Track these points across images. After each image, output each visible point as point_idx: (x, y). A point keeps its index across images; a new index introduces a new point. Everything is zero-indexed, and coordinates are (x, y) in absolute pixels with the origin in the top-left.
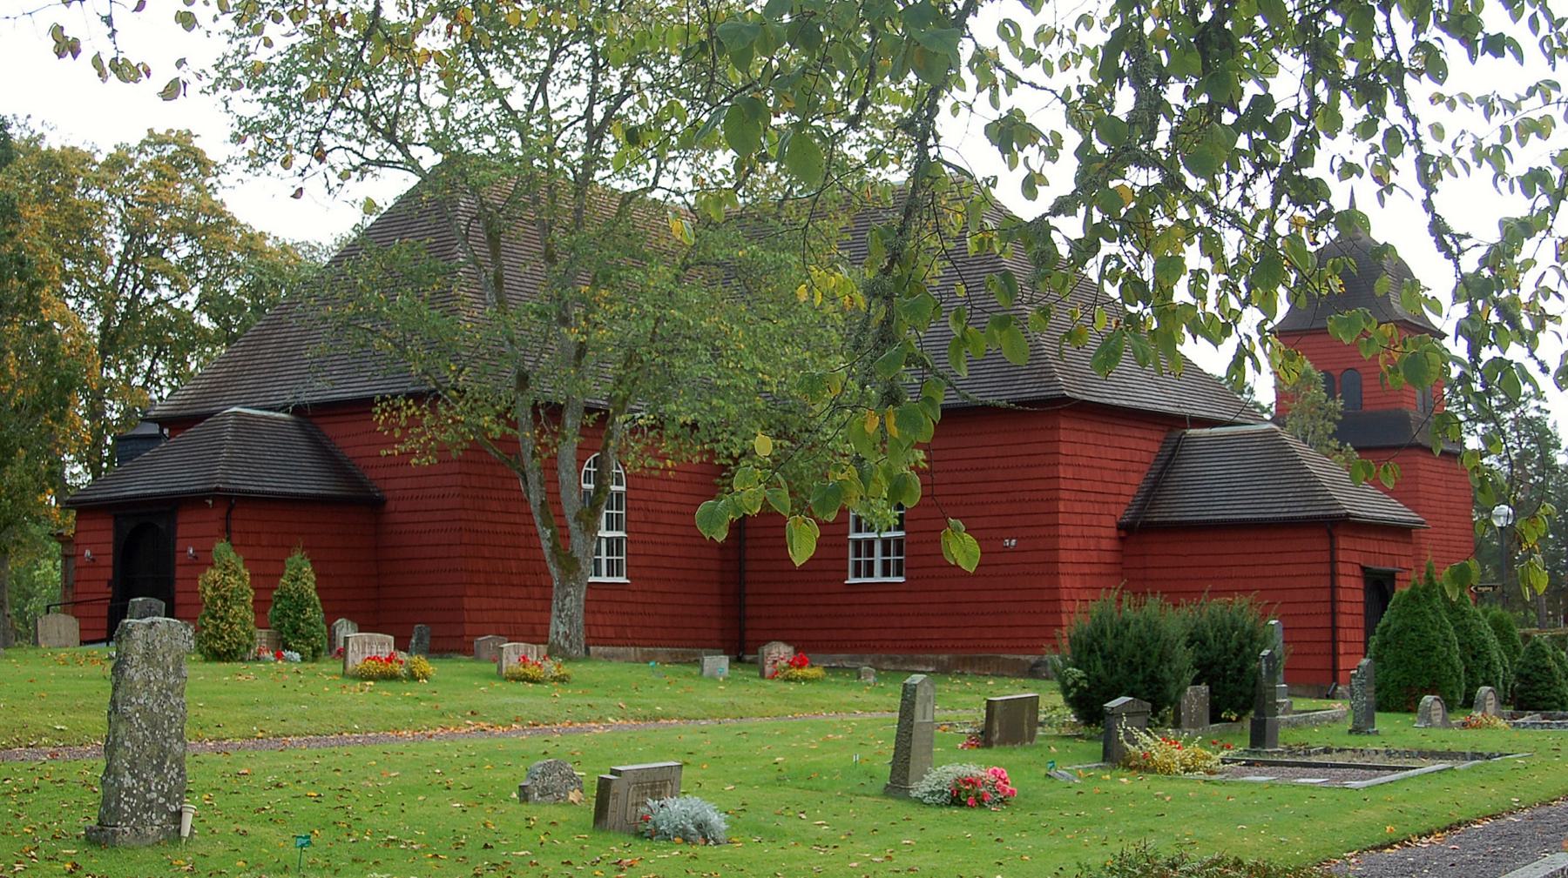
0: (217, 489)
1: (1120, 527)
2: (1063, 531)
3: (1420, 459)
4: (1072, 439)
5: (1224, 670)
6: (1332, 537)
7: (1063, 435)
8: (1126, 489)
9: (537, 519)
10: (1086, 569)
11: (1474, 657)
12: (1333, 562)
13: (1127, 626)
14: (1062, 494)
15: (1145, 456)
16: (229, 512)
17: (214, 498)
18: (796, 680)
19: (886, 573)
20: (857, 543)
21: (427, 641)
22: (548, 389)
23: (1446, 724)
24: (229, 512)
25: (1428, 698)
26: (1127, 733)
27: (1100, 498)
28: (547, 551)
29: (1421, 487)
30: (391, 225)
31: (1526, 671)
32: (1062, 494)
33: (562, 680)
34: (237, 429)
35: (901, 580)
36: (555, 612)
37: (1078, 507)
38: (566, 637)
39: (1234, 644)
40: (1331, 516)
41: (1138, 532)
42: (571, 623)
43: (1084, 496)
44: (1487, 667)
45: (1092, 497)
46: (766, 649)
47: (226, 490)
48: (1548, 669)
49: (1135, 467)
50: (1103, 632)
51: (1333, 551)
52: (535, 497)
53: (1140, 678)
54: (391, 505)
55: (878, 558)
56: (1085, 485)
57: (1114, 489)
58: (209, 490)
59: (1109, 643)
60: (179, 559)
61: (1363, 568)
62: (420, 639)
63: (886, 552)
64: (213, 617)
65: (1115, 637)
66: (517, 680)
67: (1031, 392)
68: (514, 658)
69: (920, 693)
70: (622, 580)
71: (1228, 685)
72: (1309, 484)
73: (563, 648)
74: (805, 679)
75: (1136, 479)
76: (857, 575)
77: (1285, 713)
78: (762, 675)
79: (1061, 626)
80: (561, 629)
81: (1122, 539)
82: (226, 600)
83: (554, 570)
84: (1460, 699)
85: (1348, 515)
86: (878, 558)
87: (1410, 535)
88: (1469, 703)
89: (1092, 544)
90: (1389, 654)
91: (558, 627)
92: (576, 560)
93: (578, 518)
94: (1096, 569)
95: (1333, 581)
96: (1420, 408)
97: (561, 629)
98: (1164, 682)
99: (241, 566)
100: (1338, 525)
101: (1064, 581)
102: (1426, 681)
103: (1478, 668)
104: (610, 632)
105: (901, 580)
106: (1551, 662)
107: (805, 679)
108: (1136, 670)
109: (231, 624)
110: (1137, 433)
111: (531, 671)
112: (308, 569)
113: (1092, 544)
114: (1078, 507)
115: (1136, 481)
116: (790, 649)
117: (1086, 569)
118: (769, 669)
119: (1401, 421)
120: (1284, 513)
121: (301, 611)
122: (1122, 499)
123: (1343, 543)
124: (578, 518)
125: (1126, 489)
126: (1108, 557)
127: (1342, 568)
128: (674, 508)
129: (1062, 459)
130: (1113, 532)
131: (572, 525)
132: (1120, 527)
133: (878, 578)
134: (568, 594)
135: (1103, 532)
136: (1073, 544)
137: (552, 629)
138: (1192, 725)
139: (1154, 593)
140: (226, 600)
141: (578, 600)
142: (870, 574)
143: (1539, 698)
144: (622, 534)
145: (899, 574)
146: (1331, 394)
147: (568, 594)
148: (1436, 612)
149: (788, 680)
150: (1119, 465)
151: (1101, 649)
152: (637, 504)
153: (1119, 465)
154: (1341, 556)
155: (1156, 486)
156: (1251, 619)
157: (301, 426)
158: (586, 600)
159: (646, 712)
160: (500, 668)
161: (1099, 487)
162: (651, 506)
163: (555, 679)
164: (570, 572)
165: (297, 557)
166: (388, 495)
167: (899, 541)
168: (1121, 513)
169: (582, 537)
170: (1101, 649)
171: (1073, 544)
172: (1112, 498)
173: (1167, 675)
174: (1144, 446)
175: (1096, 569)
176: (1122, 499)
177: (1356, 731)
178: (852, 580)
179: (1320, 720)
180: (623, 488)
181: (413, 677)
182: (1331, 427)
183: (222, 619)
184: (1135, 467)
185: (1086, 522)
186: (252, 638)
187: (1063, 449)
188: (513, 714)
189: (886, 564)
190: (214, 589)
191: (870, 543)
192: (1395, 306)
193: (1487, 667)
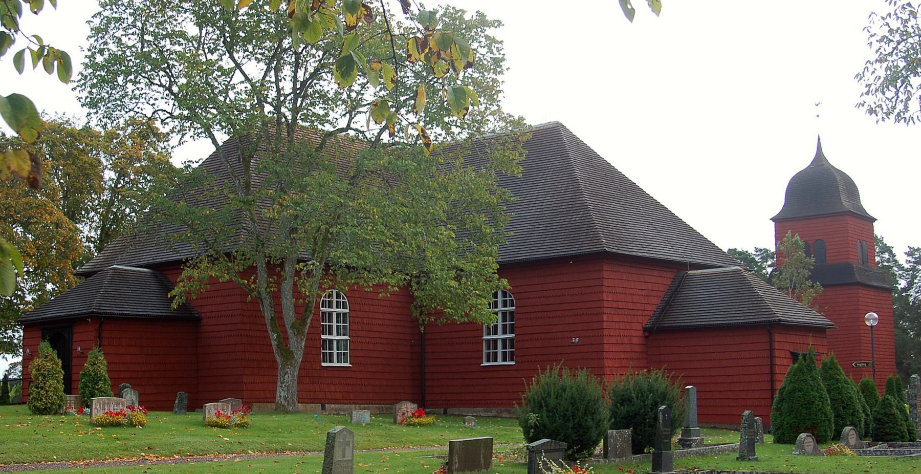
0: (92, 312)
1: (645, 330)
2: (606, 332)
3: (860, 291)
4: (611, 276)
5: (644, 419)
6: (770, 334)
7: (605, 275)
8: (648, 307)
9: (269, 328)
10: (622, 355)
11: (844, 408)
12: (772, 350)
13: (564, 390)
14: (605, 310)
15: (662, 288)
16: (101, 325)
17: (91, 317)
18: (414, 425)
19: (504, 359)
20: (488, 340)
21: (186, 402)
22: (274, 250)
23: (816, 452)
24: (101, 325)
25: (803, 435)
26: (545, 464)
27: (631, 312)
28: (274, 347)
29: (861, 307)
30: (222, 152)
31: (879, 416)
32: (605, 310)
33: (242, 426)
34: (113, 278)
35: (513, 363)
36: (279, 384)
37: (616, 318)
38: (286, 399)
39: (649, 402)
40: (769, 321)
41: (657, 333)
42: (288, 390)
43: (620, 312)
44: (853, 414)
45: (626, 312)
46: (397, 406)
47: (98, 313)
48: (893, 415)
49: (655, 293)
50: (549, 394)
51: (771, 342)
52: (268, 314)
53: (571, 425)
54: (204, 322)
55: (500, 350)
56: (621, 305)
57: (639, 306)
58: (88, 313)
59: (552, 401)
60: (74, 354)
61: (792, 353)
62: (181, 400)
63: (504, 347)
64: (37, 388)
65: (557, 398)
66: (212, 426)
67: (585, 249)
68: (214, 412)
69: (339, 440)
70: (348, 365)
71: (647, 429)
72: (757, 301)
73: (284, 406)
74: (420, 424)
75: (656, 301)
76: (488, 361)
77: (697, 446)
78: (395, 422)
79: (523, 392)
80: (283, 394)
81: (646, 337)
82: (45, 377)
83: (279, 359)
84: (830, 434)
85: (780, 320)
86: (500, 350)
87: (825, 332)
88: (837, 437)
89: (626, 340)
90: (785, 406)
91: (281, 393)
92: (292, 352)
93: (293, 327)
94: (629, 355)
95: (771, 361)
96: (860, 262)
97: (283, 394)
98: (589, 428)
99: (55, 356)
100: (773, 327)
101: (608, 363)
102: (809, 423)
103: (844, 414)
104: (338, 396)
105: (513, 363)
106: (895, 410)
107: (420, 424)
108: (569, 420)
109: (47, 391)
110: (656, 273)
111: (222, 420)
112: (102, 358)
113: (626, 340)
114: (616, 318)
115: (656, 302)
116: (415, 406)
117: (622, 355)
118: (399, 418)
119: (848, 269)
120: (741, 320)
121: (96, 384)
122: (646, 313)
123: (777, 337)
124: (293, 327)
125: (648, 307)
126: (637, 349)
127: (777, 353)
128: (380, 322)
129: (605, 289)
130: (640, 333)
131: (290, 331)
132: (645, 330)
133: (500, 362)
134: (287, 373)
135: (634, 333)
136: (614, 340)
137: (278, 394)
138: (616, 456)
139: (582, 368)
140: (45, 377)
141: (293, 376)
142: (496, 360)
143: (887, 434)
144: (347, 337)
145: (512, 360)
146: (808, 255)
147: (287, 373)
148: (814, 379)
149: (409, 425)
150: (644, 293)
151: (547, 406)
152: (357, 320)
153: (644, 293)
154: (777, 345)
155: (667, 306)
156: (664, 386)
157: (155, 276)
158: (299, 376)
159: (279, 447)
160: (204, 418)
161: (631, 306)
162: (365, 321)
163: (237, 425)
164: (288, 359)
165: (96, 351)
166: (203, 315)
167: (512, 340)
168: (646, 321)
169: (295, 339)
170: (547, 406)
171: (614, 340)
172: (640, 312)
173: (590, 423)
174: (661, 281)
175: (629, 355)
176: (646, 313)
177: (741, 458)
178: (485, 364)
179: (723, 451)
180: (347, 311)
181: (132, 425)
182: (807, 273)
183: (42, 388)
184: (655, 293)
185: (622, 329)
186: (62, 400)
187: (606, 283)
188: (179, 448)
189: (504, 354)
190: (38, 370)
191: (495, 341)
192: (844, 203)
193: (853, 414)
